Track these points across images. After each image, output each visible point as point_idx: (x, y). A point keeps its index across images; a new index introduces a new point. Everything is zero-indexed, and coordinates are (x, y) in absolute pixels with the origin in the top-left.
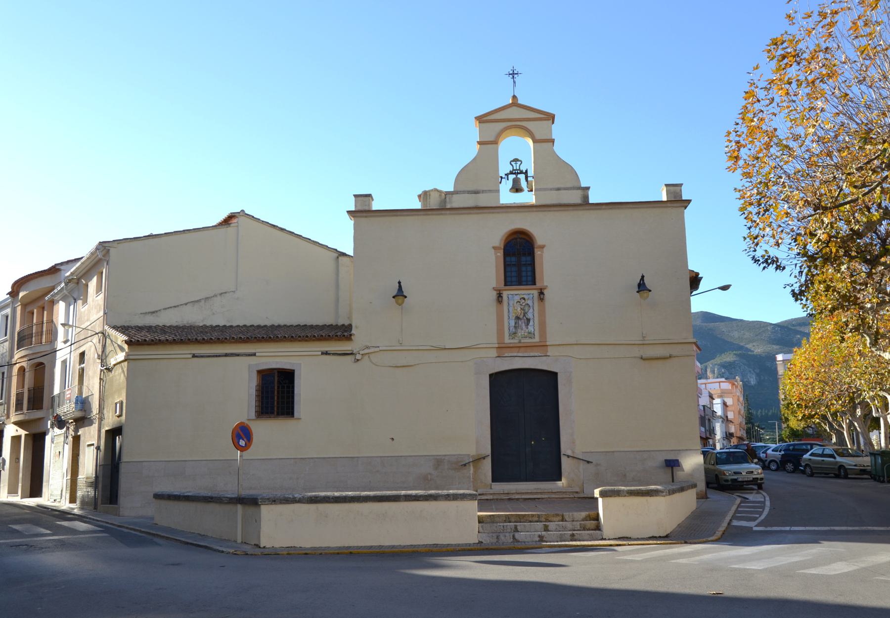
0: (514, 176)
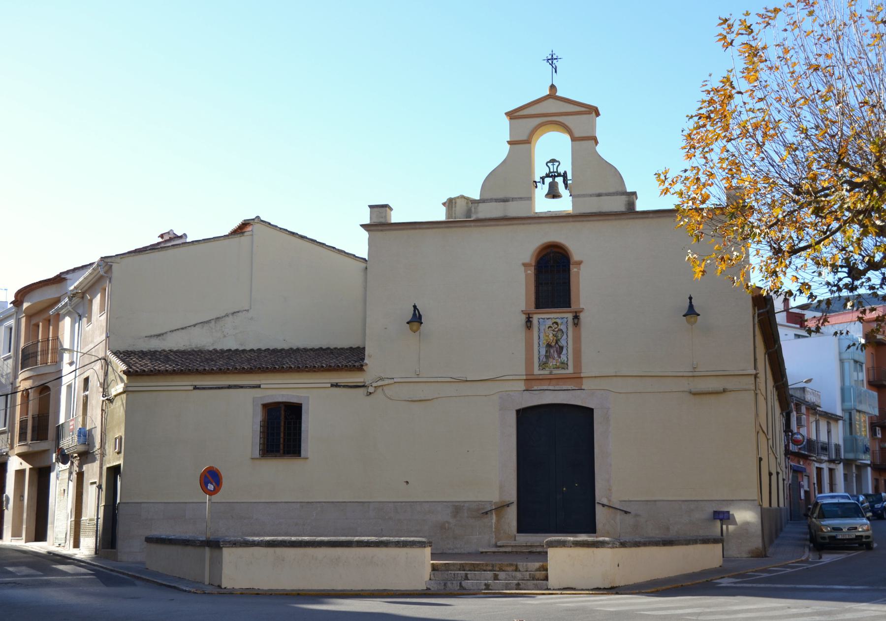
0: (550, 180)
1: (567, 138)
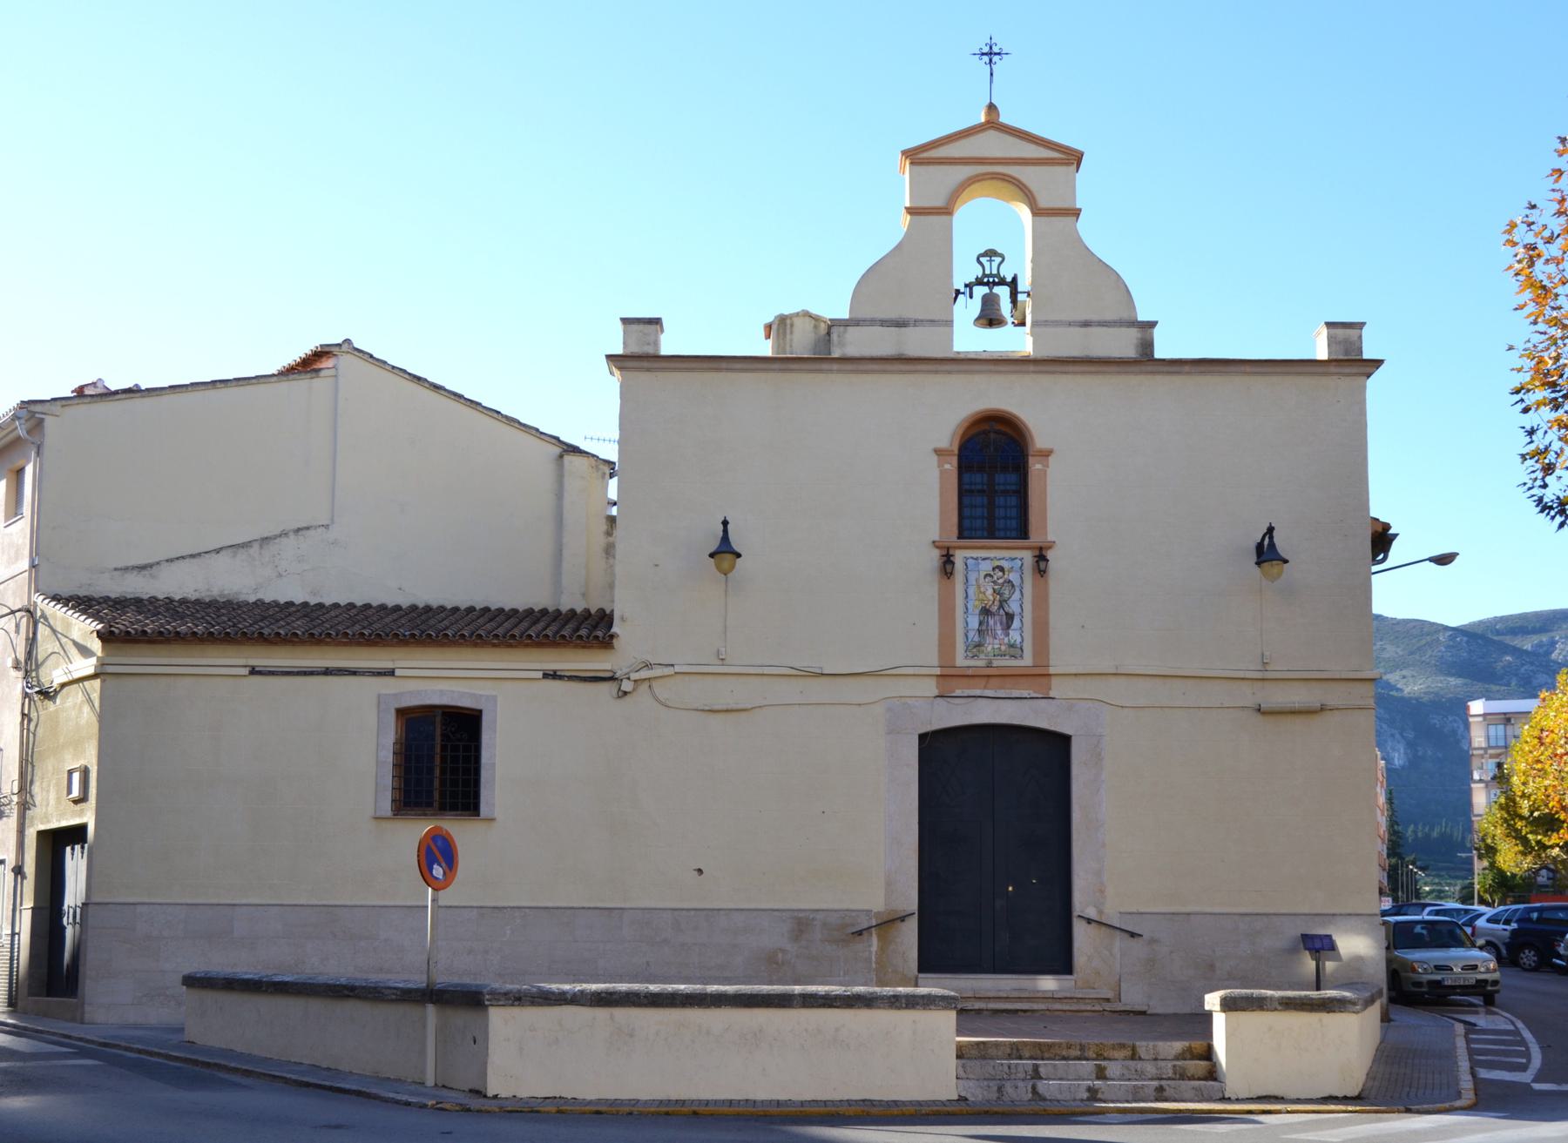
0: (985, 290)
1: (1024, 212)
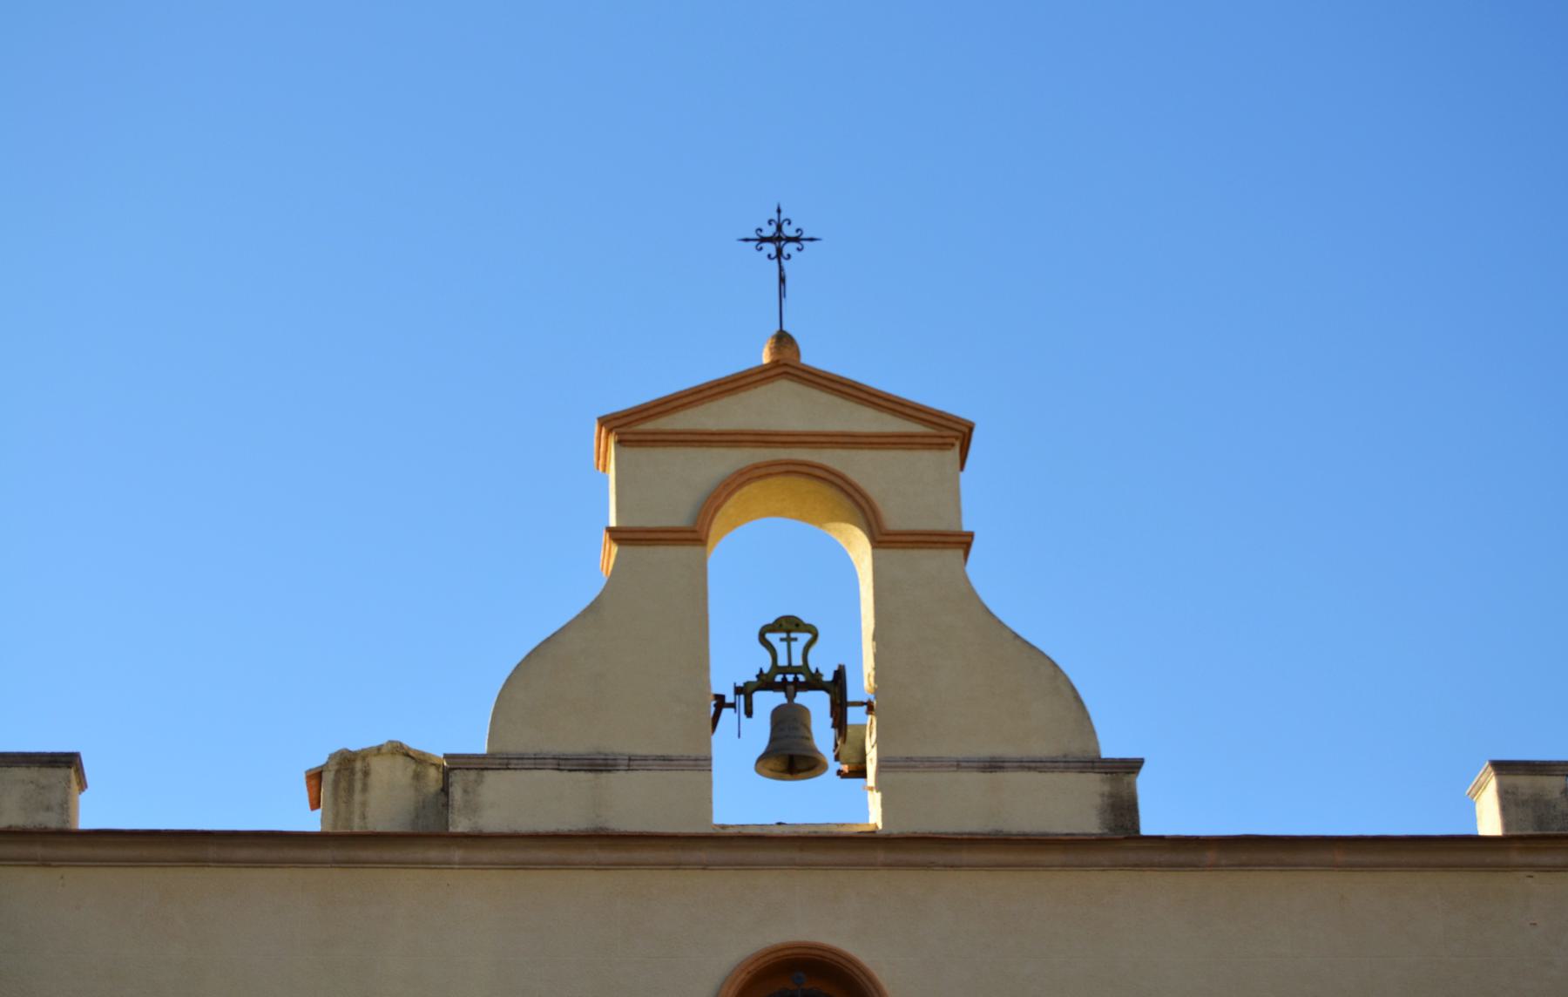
0: (779, 698)
